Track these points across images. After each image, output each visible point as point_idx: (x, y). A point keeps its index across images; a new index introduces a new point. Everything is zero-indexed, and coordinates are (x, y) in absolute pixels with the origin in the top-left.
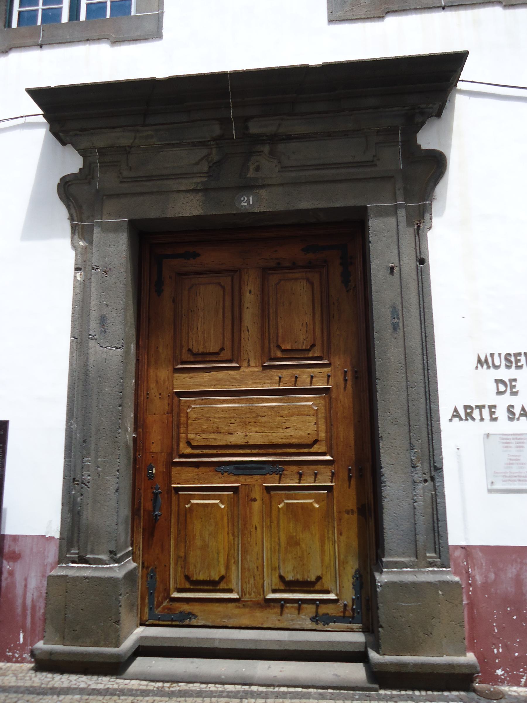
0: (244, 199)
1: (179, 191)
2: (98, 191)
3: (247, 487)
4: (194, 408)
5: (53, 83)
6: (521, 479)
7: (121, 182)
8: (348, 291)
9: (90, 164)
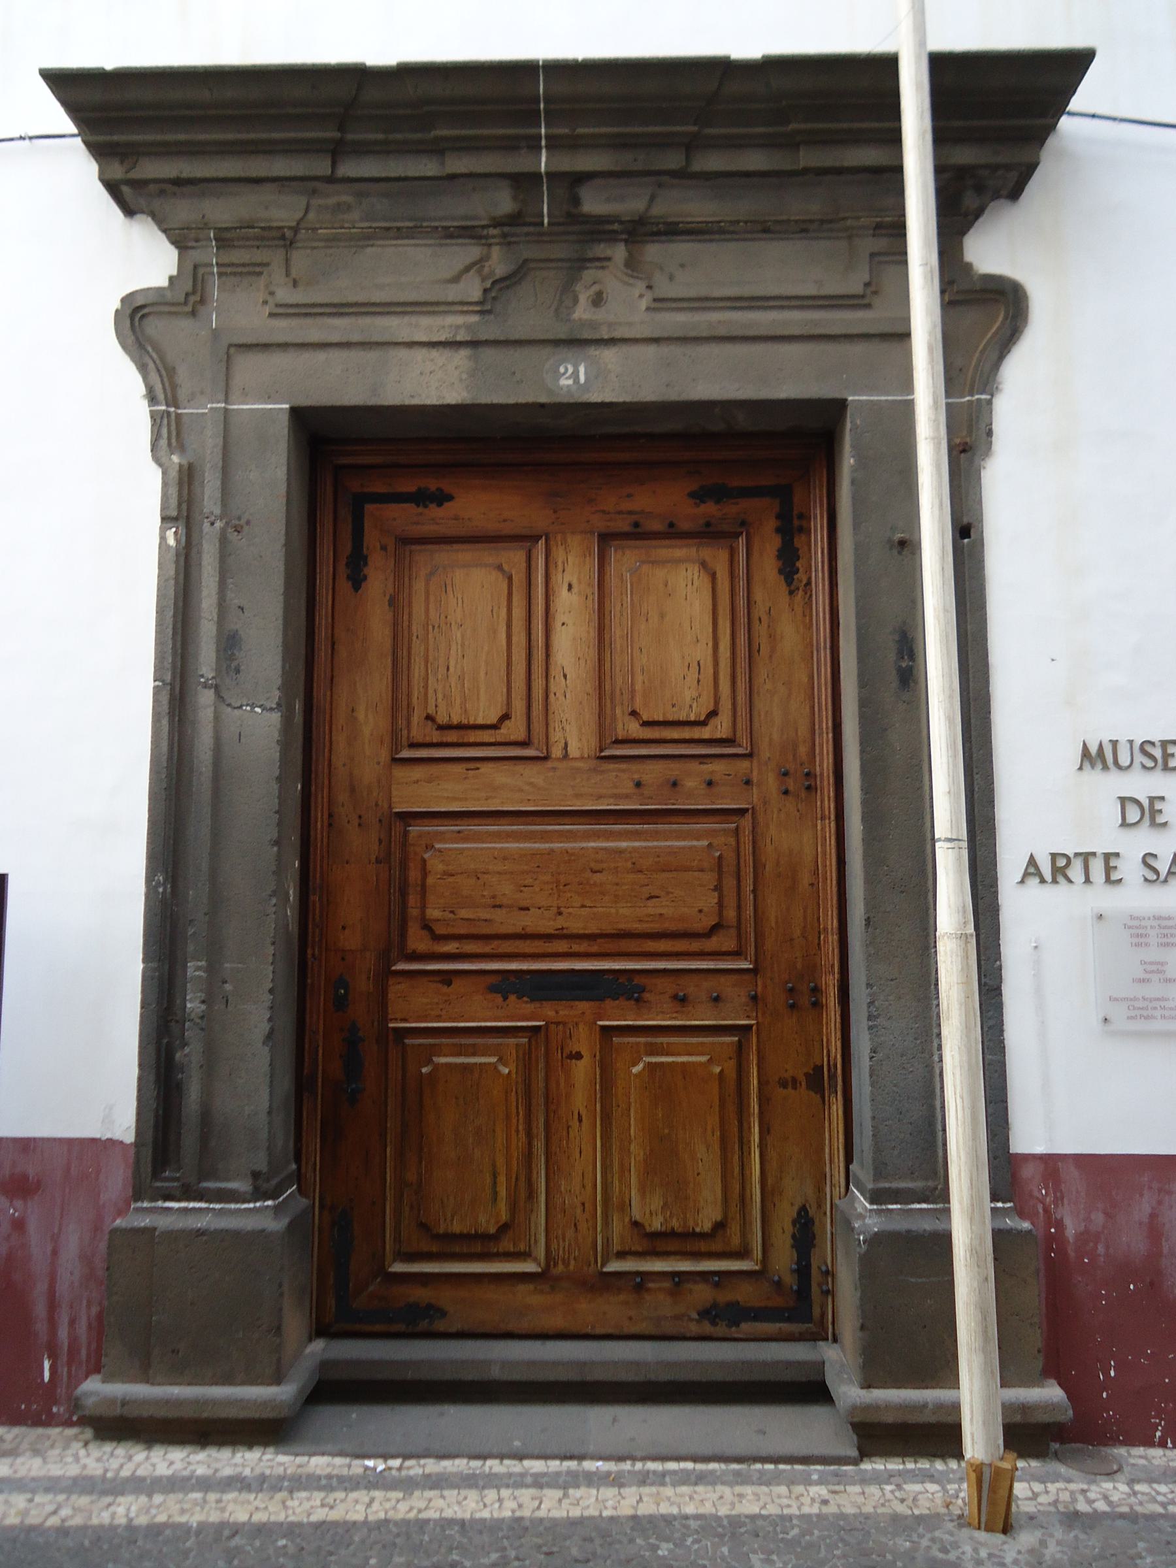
0: (567, 370)
2: (216, 334)
3: (561, 1027)
4: (440, 851)
5: (110, 60)
7: (271, 315)
8: (791, 593)
9: (195, 267)
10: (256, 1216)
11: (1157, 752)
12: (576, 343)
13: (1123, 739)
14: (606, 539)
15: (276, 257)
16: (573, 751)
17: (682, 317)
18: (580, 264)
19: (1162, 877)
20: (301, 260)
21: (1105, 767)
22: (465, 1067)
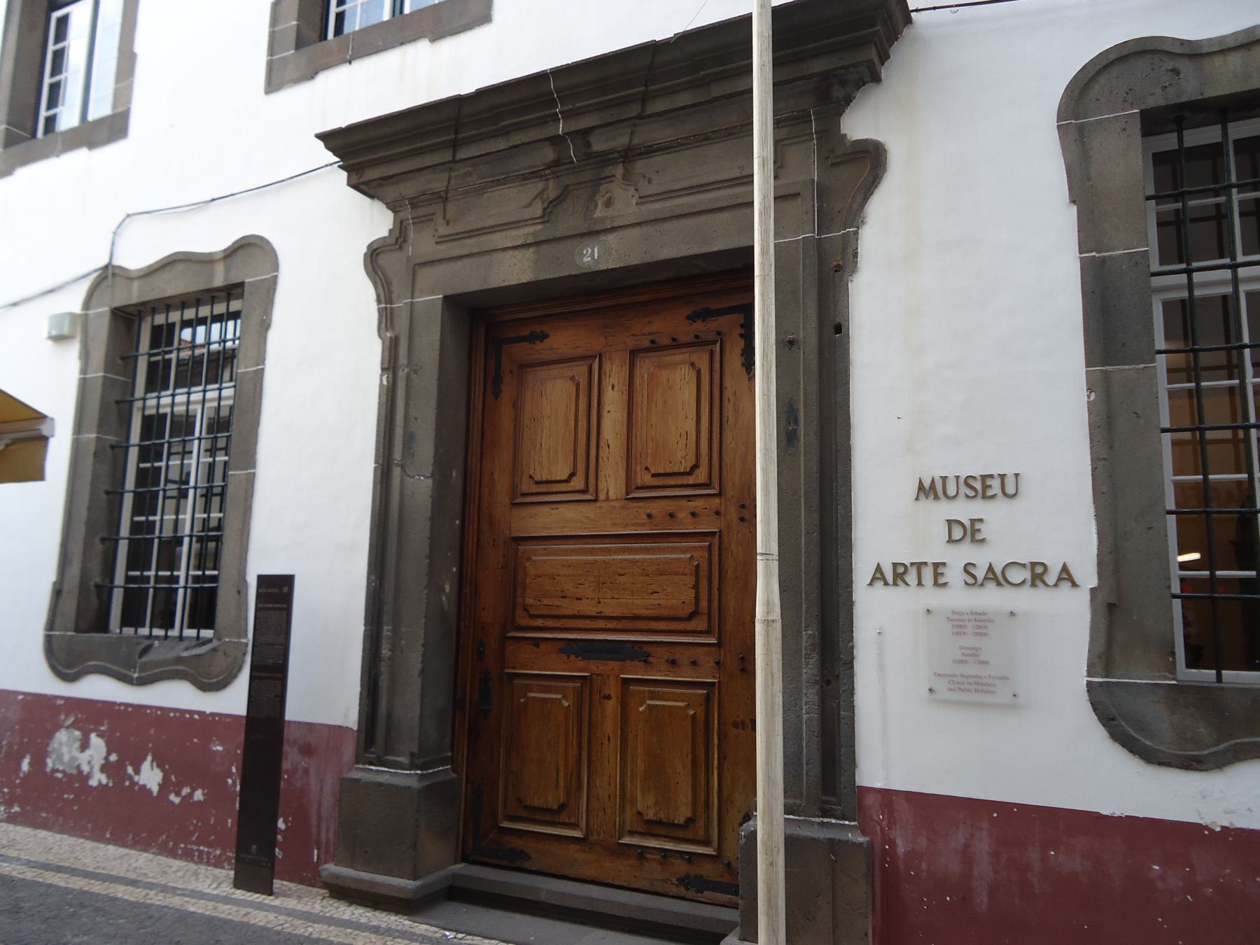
1: (504, 249)
6: (980, 688)
10: (407, 778)
11: (978, 485)
12: (593, 234)
13: (951, 475)
14: (634, 353)
15: (438, 208)
16: (612, 495)
17: (657, 206)
18: (598, 182)
19: (980, 581)
20: (452, 208)
21: (936, 497)
22: (544, 700)
